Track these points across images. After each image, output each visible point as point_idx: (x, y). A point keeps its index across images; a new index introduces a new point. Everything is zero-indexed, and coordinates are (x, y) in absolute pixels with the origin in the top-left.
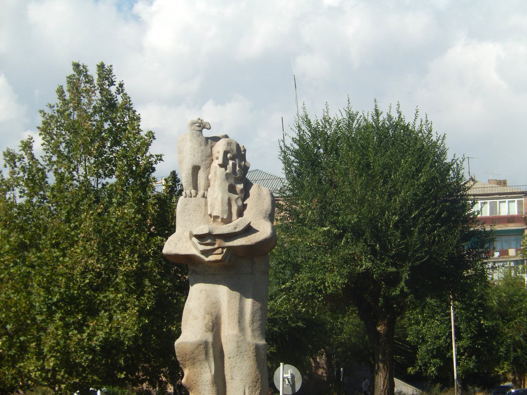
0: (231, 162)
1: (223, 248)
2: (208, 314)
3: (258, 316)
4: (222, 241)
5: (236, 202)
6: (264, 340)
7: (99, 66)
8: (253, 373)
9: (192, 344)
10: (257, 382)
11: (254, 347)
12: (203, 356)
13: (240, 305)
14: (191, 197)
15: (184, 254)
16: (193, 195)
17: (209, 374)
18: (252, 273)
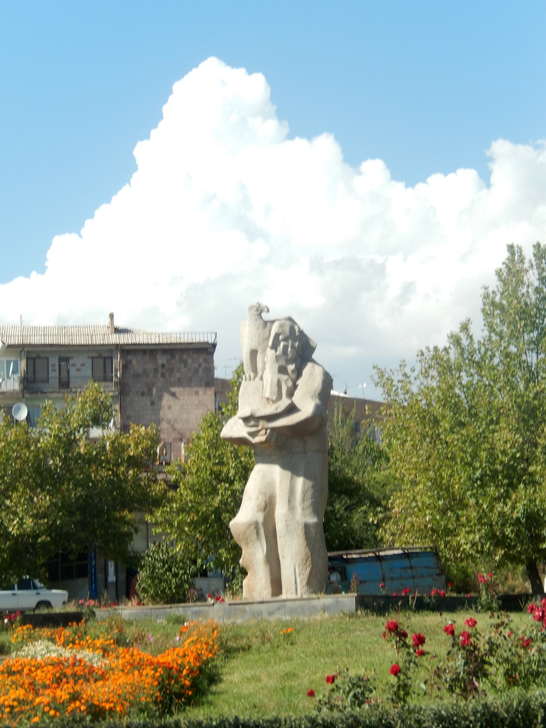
0: (282, 344)
1: (266, 429)
7: (534, 246)
12: (255, 536)
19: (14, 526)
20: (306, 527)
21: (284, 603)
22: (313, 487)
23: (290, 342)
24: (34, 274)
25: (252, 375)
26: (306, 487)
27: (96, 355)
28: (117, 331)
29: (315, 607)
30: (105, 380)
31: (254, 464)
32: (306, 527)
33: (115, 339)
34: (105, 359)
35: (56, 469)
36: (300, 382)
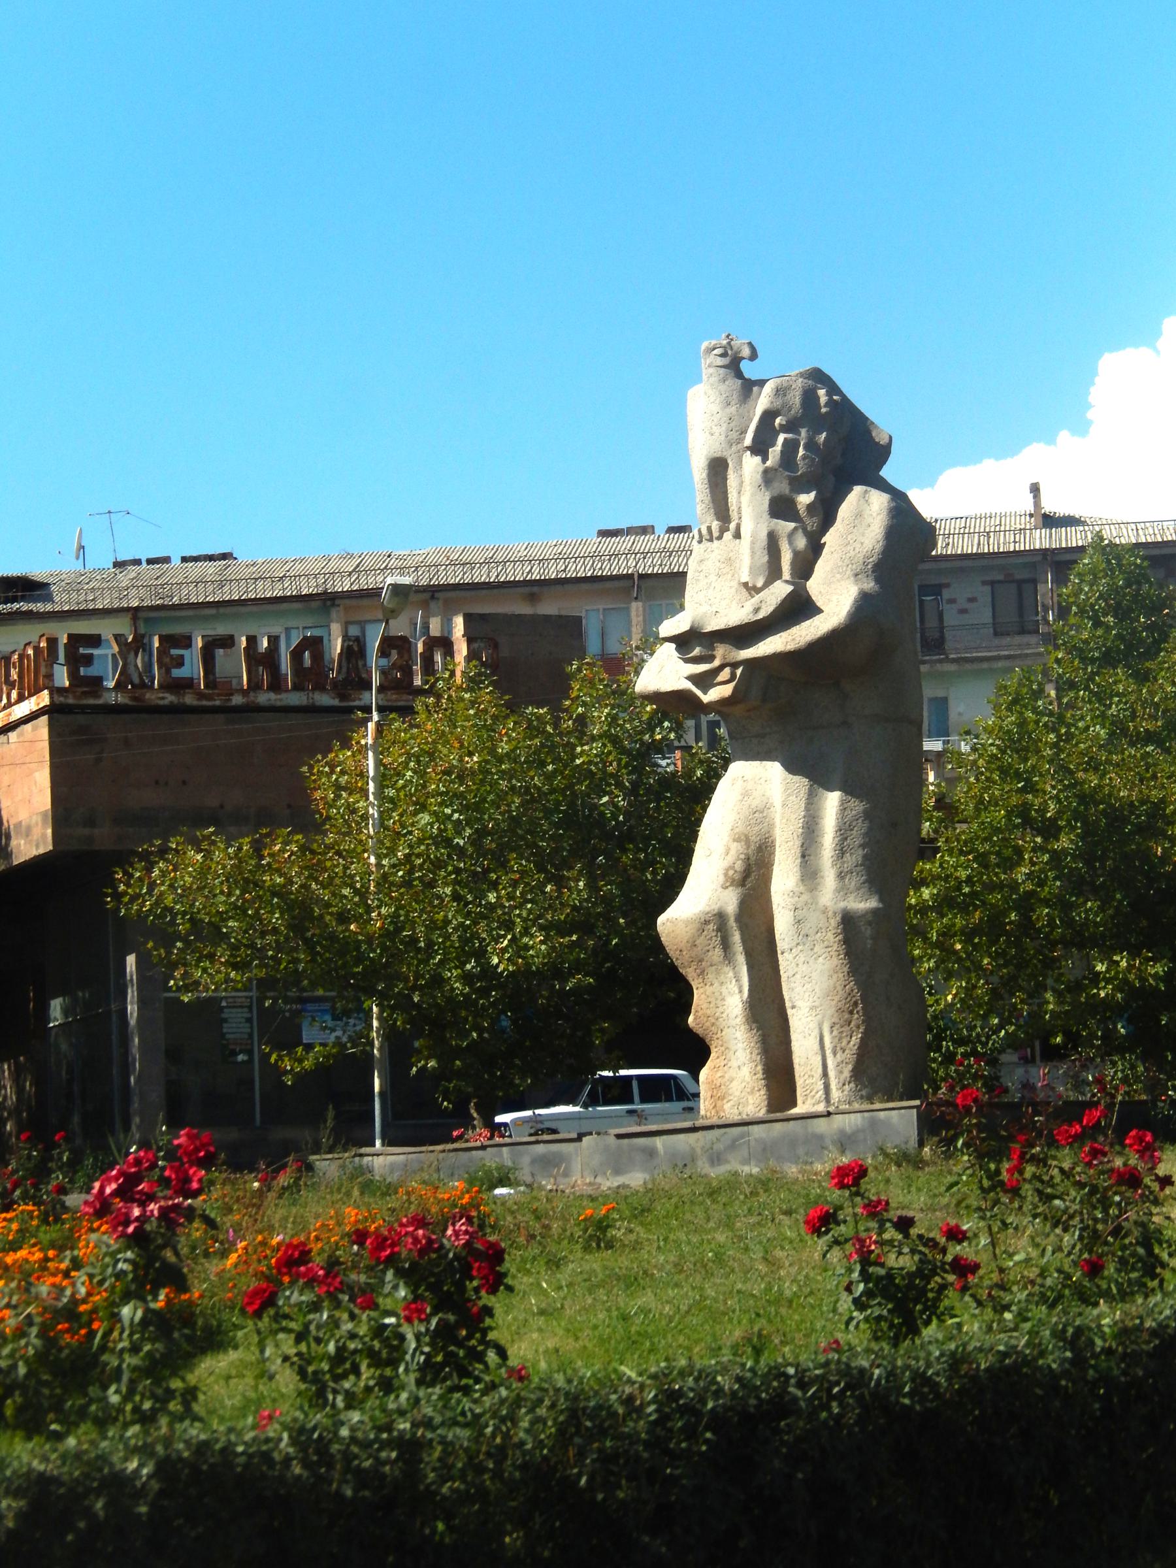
0: (781, 437)
1: (734, 665)
5: (790, 543)
6: (876, 897)
8: (839, 988)
9: (687, 922)
10: (851, 1012)
11: (838, 918)
13: (807, 809)
14: (711, 540)
15: (669, 689)
16: (716, 534)
19: (504, 950)
20: (848, 921)
21: (746, 1128)
22: (867, 815)
23: (803, 432)
24: (1064, 436)
25: (715, 525)
26: (850, 814)
27: (1000, 577)
28: (1050, 521)
29: (820, 1138)
30: (1023, 631)
31: (726, 763)
32: (848, 921)
33: (1041, 539)
34: (1020, 583)
35: (614, 817)
36: (829, 538)
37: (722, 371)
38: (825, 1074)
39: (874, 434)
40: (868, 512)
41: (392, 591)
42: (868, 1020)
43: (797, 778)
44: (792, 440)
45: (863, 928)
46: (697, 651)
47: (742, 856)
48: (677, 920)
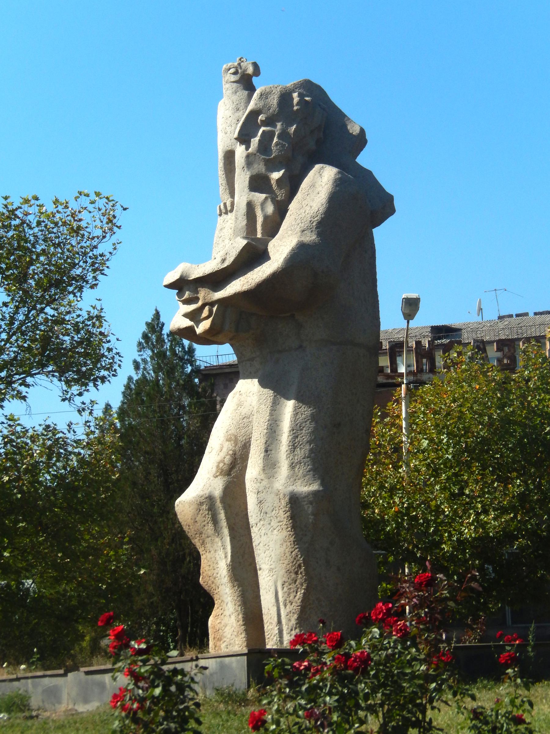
2: (228, 440)
3: (305, 435)
4: (207, 290)
5: (263, 209)
6: (319, 482)
8: (288, 554)
12: (210, 526)
13: (271, 415)
14: (226, 213)
16: (229, 208)
17: (224, 561)
18: (301, 347)
20: (294, 501)
22: (313, 418)
23: (279, 125)
26: (301, 417)
32: (294, 501)
36: (293, 207)
37: (235, 84)
38: (279, 622)
39: (349, 127)
40: (320, 183)
41: (406, 303)
42: (309, 578)
43: (266, 391)
44: (269, 132)
45: (306, 507)
46: (187, 295)
47: (231, 452)
48: (186, 502)
